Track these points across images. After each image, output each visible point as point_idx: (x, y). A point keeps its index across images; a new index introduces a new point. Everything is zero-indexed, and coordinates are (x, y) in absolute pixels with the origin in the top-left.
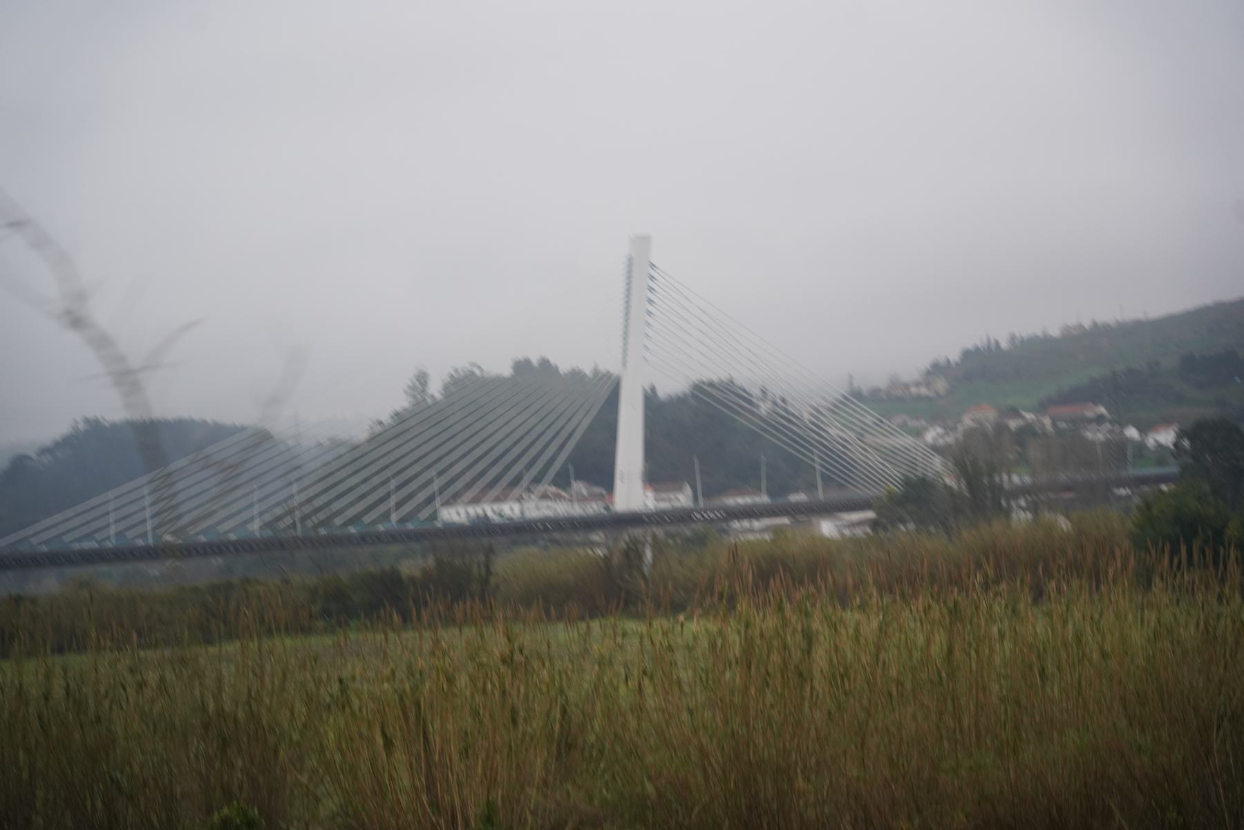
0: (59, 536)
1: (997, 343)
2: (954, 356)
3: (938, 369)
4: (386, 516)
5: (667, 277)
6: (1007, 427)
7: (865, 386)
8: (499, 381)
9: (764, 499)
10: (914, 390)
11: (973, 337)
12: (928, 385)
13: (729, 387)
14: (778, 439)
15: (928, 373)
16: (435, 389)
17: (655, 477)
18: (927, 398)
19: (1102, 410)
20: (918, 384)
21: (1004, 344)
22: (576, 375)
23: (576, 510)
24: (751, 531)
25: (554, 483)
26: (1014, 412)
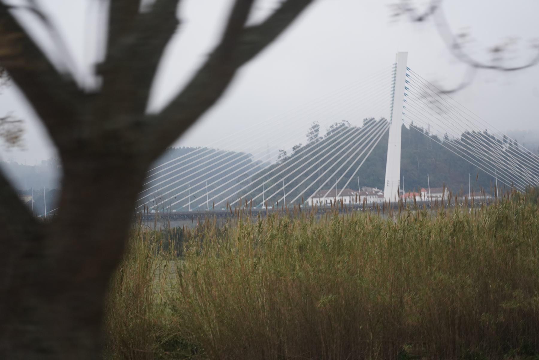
16: (322, 133)
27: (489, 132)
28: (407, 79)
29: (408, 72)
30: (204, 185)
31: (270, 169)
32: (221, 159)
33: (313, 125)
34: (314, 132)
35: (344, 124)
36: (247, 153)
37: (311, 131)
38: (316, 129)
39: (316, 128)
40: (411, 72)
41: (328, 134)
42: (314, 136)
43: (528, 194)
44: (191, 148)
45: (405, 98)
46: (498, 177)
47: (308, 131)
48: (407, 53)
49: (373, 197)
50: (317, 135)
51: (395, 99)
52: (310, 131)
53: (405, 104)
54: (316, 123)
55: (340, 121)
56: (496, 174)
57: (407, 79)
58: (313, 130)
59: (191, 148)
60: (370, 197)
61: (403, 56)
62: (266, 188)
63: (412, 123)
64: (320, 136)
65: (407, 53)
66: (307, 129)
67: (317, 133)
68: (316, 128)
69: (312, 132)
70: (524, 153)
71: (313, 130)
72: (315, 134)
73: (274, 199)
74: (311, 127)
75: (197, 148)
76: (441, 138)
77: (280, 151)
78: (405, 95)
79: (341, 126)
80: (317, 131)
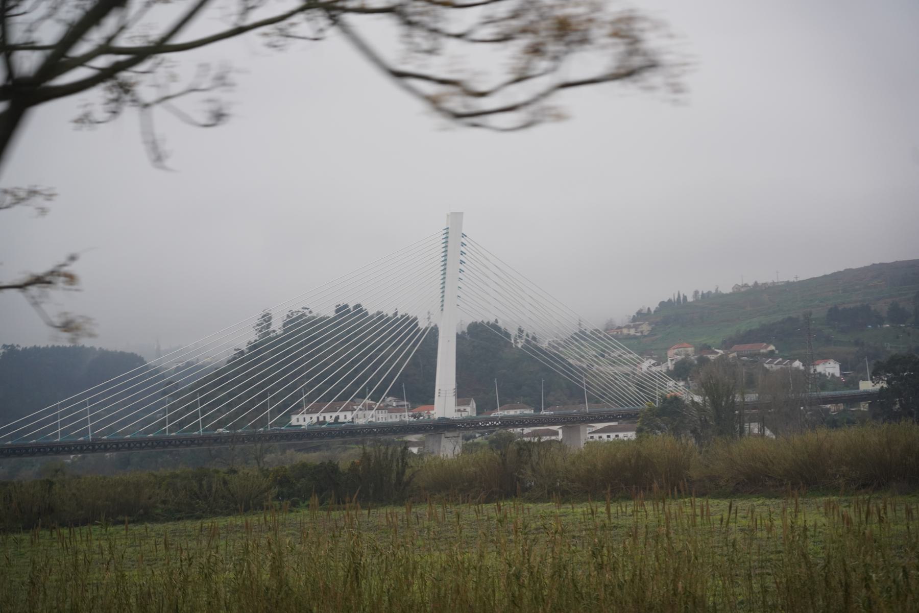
0: (111, 429)
1: (685, 298)
2: (654, 306)
3: (641, 316)
4: (263, 422)
5: (472, 243)
6: (708, 360)
7: (589, 327)
8: (323, 321)
9: (529, 412)
10: (625, 331)
11: (668, 294)
12: (636, 327)
13: (495, 326)
14: (122, 379)
15: (634, 319)
16: (277, 326)
17: (462, 394)
18: (635, 337)
19: (772, 347)
20: (628, 327)
21: (690, 299)
22: (380, 316)
23: (394, 418)
24: (522, 435)
25: (372, 398)
26: (708, 348)
27: (500, 324)
30: (84, 404)
31: (217, 374)
32: (425, 333)
39: (267, 319)
40: (469, 240)
41: (284, 325)
46: (587, 388)
49: (382, 413)
51: (447, 276)
54: (267, 311)
56: (585, 384)
60: (378, 413)
62: (164, 410)
64: (272, 328)
65: (462, 214)
66: (255, 317)
68: (267, 319)
70: (627, 364)
73: (181, 424)
77: (235, 350)
78: (461, 271)
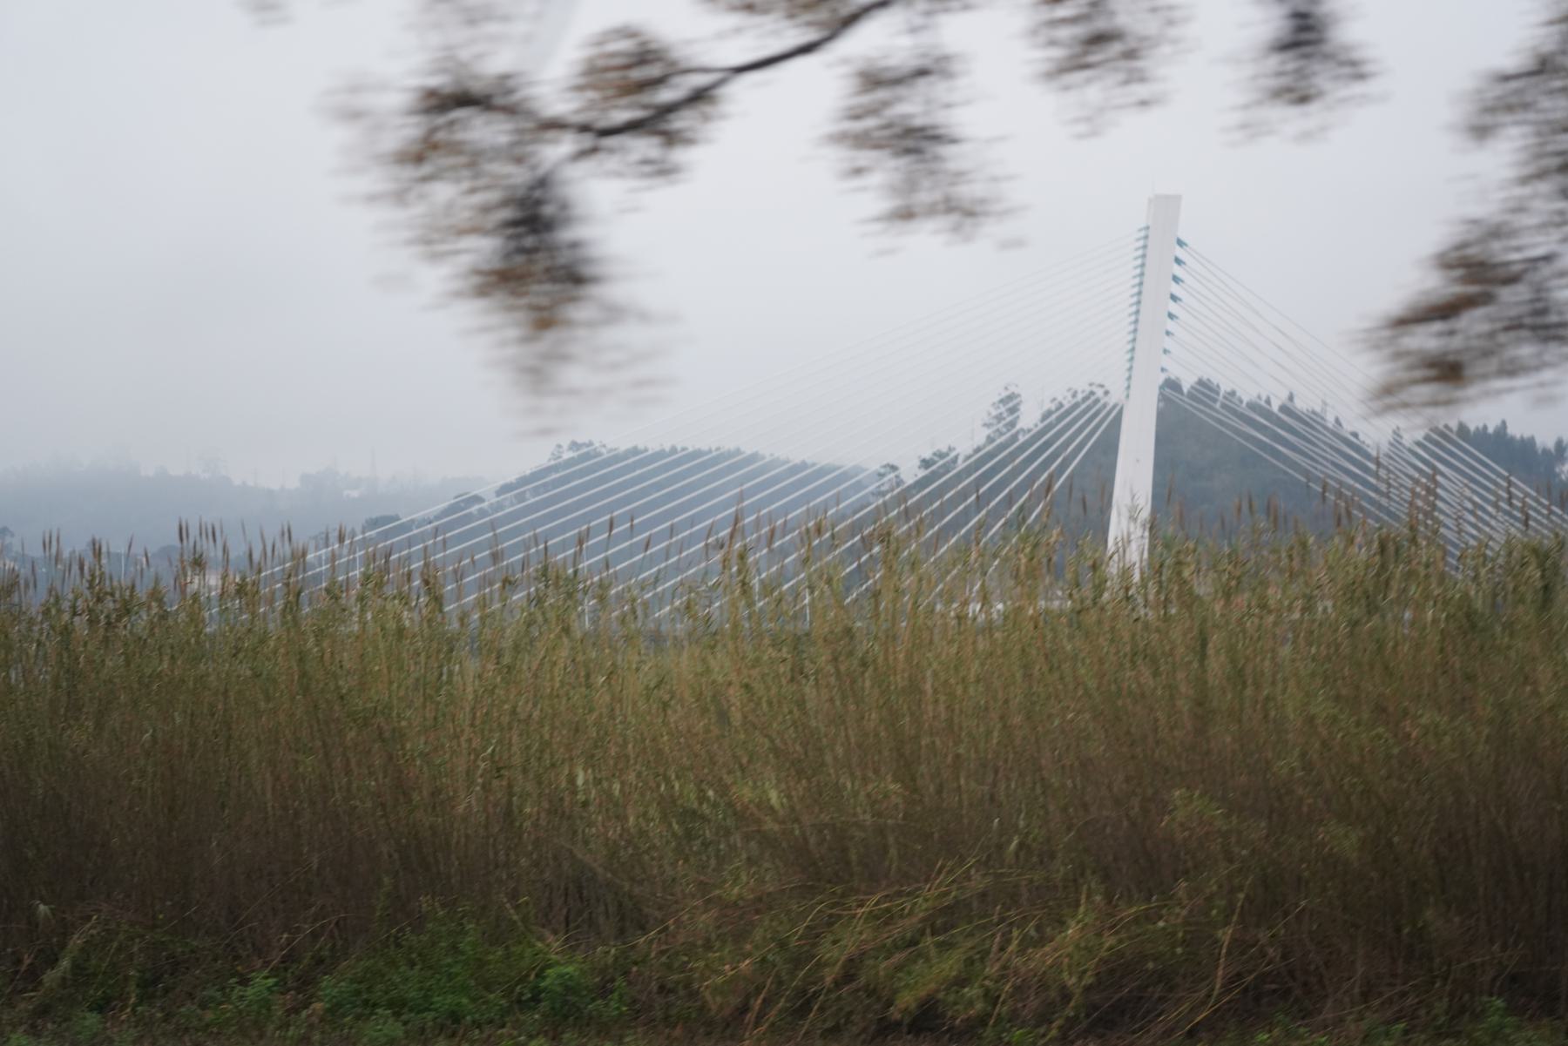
16: (1029, 419)
28: (1178, 270)
29: (1180, 253)
33: (1005, 394)
34: (1005, 415)
35: (1092, 393)
36: (824, 463)
37: (999, 411)
38: (1011, 405)
39: (1011, 403)
42: (1005, 425)
43: (661, 770)
44: (1522, 437)
45: (1170, 325)
47: (989, 414)
48: (1178, 198)
50: (1012, 424)
52: (994, 413)
53: (1168, 343)
54: (1012, 389)
55: (1082, 387)
57: (1178, 270)
58: (1003, 409)
59: (1522, 437)
61: (1166, 206)
63: (1291, 398)
65: (1178, 198)
67: (1015, 415)
68: (1011, 403)
69: (1001, 414)
71: (1003, 409)
72: (1009, 419)
74: (997, 398)
75: (710, 451)
76: (1518, 436)
79: (1085, 399)
80: (1013, 410)
